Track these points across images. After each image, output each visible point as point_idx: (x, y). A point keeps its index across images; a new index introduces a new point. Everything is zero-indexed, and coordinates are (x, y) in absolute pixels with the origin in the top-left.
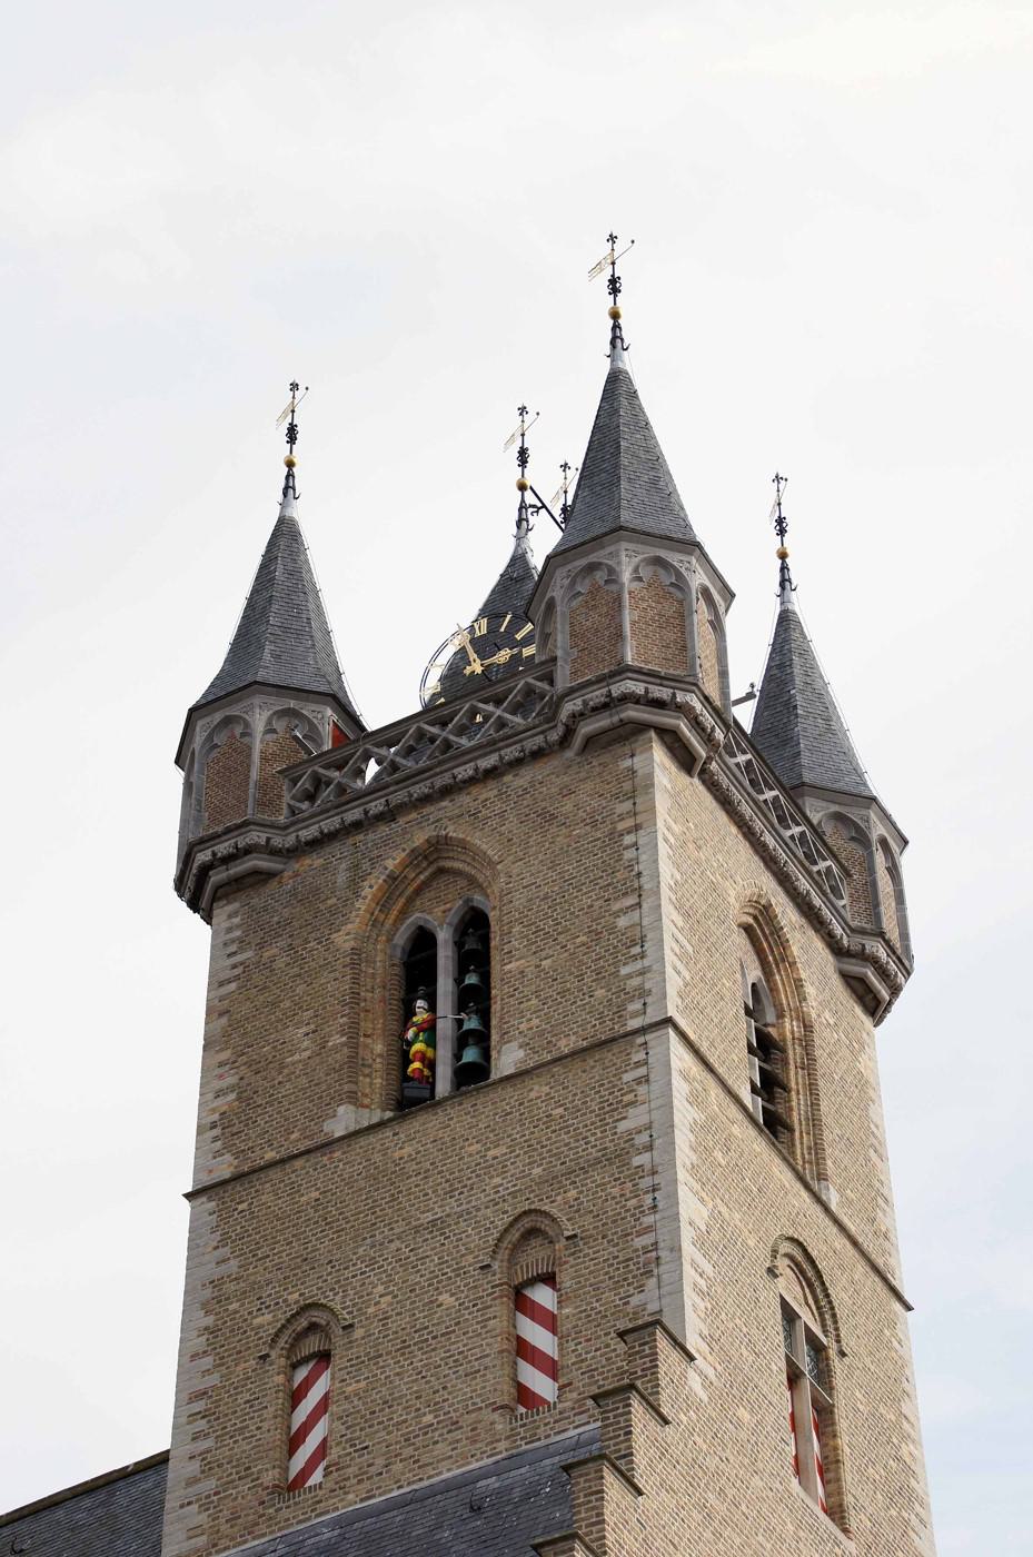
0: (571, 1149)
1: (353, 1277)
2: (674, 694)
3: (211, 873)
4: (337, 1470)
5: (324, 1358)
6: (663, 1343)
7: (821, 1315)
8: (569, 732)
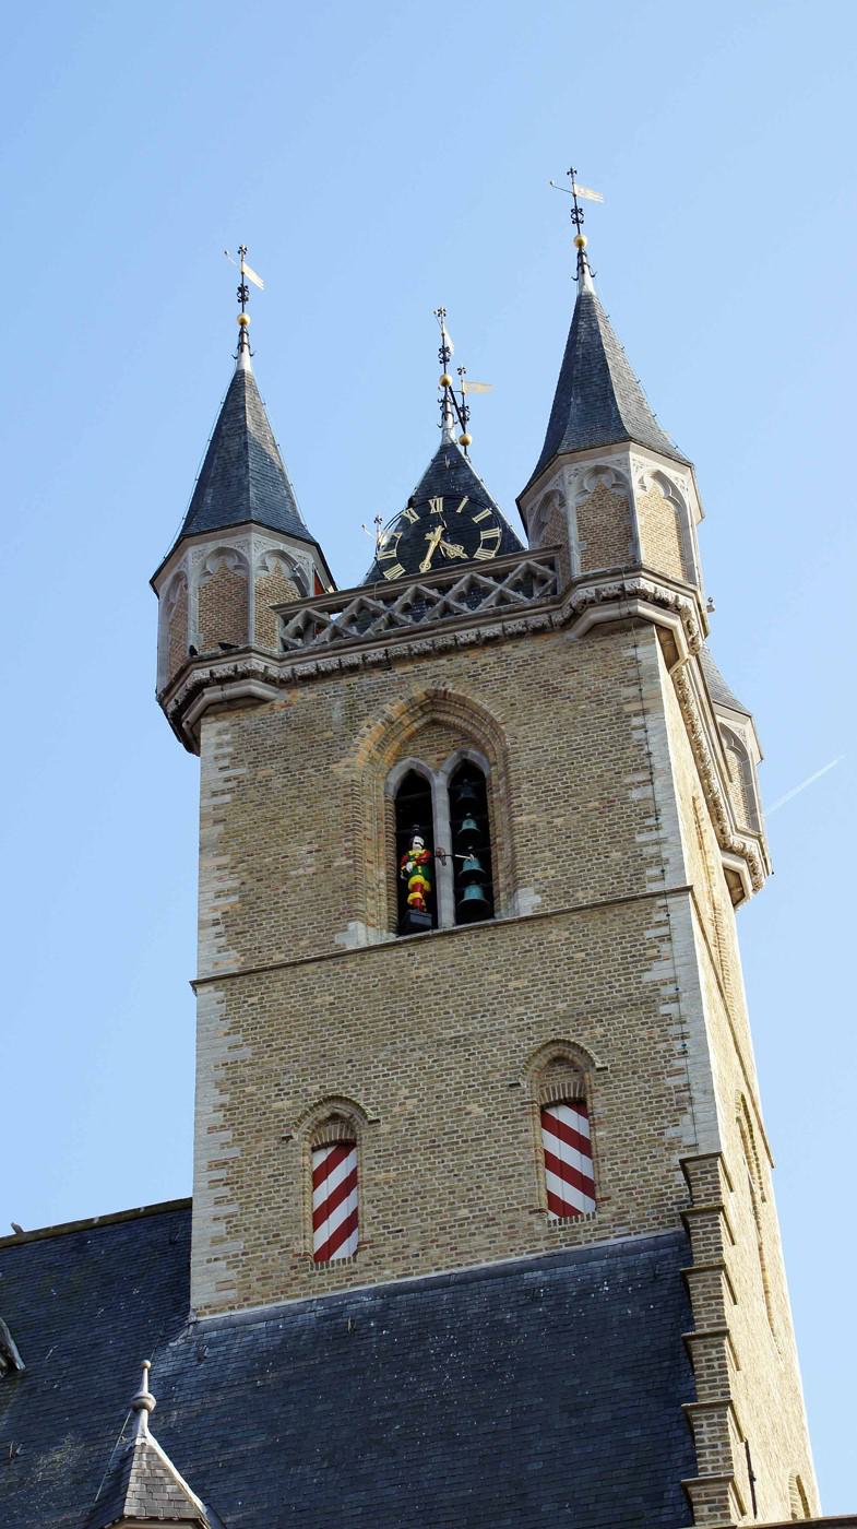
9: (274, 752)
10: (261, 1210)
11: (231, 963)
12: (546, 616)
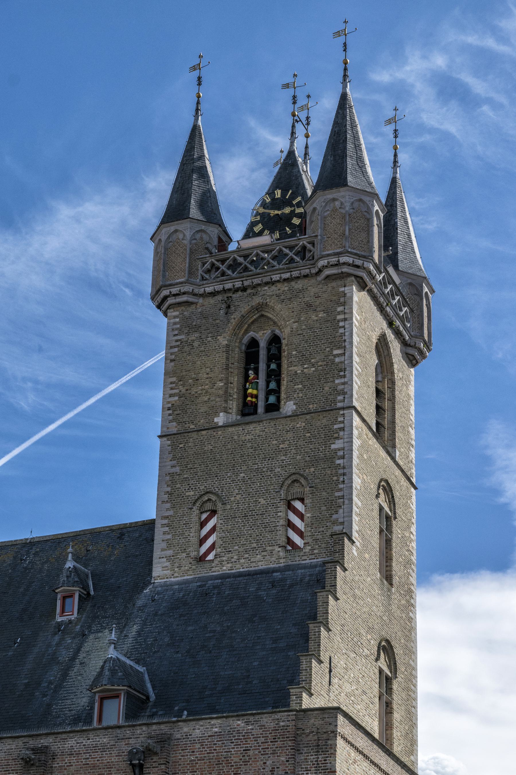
0: (312, 451)
1: (226, 484)
2: (363, 263)
3: (168, 299)
4: (219, 557)
5: (214, 512)
6: (346, 540)
7: (390, 504)
8: (320, 271)
9: (197, 328)
10: (180, 538)
11: (174, 428)
12: (309, 270)
